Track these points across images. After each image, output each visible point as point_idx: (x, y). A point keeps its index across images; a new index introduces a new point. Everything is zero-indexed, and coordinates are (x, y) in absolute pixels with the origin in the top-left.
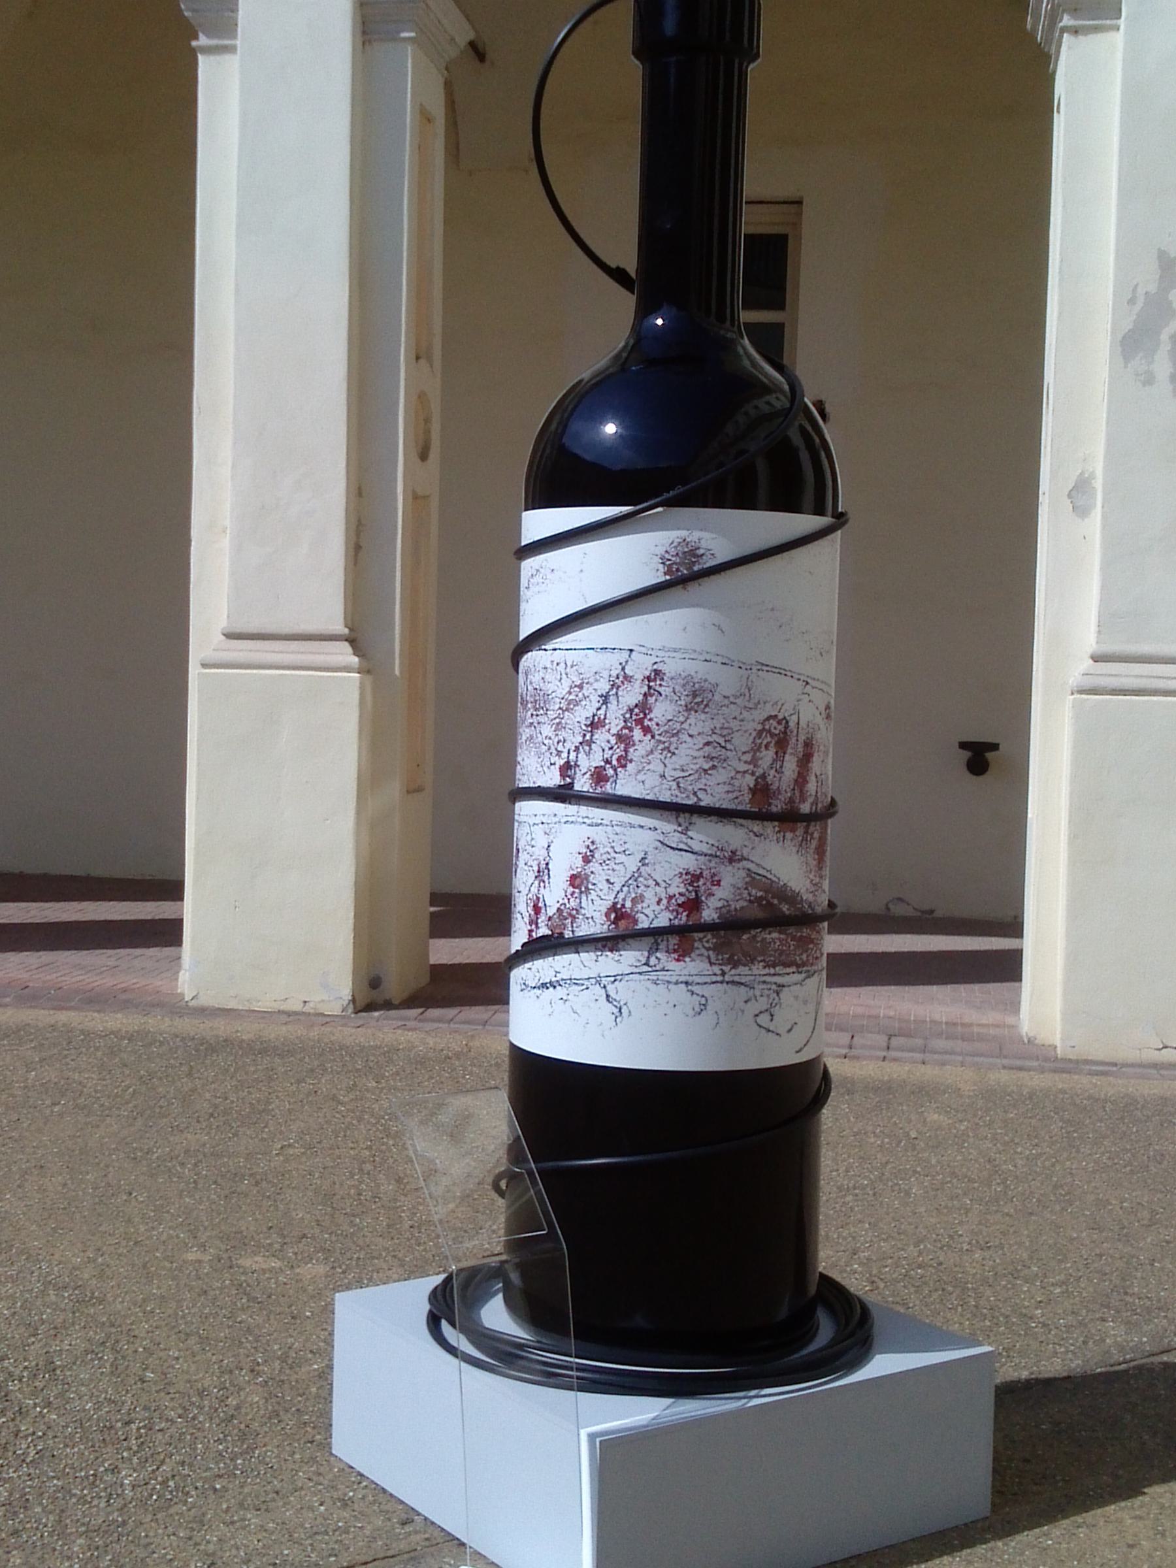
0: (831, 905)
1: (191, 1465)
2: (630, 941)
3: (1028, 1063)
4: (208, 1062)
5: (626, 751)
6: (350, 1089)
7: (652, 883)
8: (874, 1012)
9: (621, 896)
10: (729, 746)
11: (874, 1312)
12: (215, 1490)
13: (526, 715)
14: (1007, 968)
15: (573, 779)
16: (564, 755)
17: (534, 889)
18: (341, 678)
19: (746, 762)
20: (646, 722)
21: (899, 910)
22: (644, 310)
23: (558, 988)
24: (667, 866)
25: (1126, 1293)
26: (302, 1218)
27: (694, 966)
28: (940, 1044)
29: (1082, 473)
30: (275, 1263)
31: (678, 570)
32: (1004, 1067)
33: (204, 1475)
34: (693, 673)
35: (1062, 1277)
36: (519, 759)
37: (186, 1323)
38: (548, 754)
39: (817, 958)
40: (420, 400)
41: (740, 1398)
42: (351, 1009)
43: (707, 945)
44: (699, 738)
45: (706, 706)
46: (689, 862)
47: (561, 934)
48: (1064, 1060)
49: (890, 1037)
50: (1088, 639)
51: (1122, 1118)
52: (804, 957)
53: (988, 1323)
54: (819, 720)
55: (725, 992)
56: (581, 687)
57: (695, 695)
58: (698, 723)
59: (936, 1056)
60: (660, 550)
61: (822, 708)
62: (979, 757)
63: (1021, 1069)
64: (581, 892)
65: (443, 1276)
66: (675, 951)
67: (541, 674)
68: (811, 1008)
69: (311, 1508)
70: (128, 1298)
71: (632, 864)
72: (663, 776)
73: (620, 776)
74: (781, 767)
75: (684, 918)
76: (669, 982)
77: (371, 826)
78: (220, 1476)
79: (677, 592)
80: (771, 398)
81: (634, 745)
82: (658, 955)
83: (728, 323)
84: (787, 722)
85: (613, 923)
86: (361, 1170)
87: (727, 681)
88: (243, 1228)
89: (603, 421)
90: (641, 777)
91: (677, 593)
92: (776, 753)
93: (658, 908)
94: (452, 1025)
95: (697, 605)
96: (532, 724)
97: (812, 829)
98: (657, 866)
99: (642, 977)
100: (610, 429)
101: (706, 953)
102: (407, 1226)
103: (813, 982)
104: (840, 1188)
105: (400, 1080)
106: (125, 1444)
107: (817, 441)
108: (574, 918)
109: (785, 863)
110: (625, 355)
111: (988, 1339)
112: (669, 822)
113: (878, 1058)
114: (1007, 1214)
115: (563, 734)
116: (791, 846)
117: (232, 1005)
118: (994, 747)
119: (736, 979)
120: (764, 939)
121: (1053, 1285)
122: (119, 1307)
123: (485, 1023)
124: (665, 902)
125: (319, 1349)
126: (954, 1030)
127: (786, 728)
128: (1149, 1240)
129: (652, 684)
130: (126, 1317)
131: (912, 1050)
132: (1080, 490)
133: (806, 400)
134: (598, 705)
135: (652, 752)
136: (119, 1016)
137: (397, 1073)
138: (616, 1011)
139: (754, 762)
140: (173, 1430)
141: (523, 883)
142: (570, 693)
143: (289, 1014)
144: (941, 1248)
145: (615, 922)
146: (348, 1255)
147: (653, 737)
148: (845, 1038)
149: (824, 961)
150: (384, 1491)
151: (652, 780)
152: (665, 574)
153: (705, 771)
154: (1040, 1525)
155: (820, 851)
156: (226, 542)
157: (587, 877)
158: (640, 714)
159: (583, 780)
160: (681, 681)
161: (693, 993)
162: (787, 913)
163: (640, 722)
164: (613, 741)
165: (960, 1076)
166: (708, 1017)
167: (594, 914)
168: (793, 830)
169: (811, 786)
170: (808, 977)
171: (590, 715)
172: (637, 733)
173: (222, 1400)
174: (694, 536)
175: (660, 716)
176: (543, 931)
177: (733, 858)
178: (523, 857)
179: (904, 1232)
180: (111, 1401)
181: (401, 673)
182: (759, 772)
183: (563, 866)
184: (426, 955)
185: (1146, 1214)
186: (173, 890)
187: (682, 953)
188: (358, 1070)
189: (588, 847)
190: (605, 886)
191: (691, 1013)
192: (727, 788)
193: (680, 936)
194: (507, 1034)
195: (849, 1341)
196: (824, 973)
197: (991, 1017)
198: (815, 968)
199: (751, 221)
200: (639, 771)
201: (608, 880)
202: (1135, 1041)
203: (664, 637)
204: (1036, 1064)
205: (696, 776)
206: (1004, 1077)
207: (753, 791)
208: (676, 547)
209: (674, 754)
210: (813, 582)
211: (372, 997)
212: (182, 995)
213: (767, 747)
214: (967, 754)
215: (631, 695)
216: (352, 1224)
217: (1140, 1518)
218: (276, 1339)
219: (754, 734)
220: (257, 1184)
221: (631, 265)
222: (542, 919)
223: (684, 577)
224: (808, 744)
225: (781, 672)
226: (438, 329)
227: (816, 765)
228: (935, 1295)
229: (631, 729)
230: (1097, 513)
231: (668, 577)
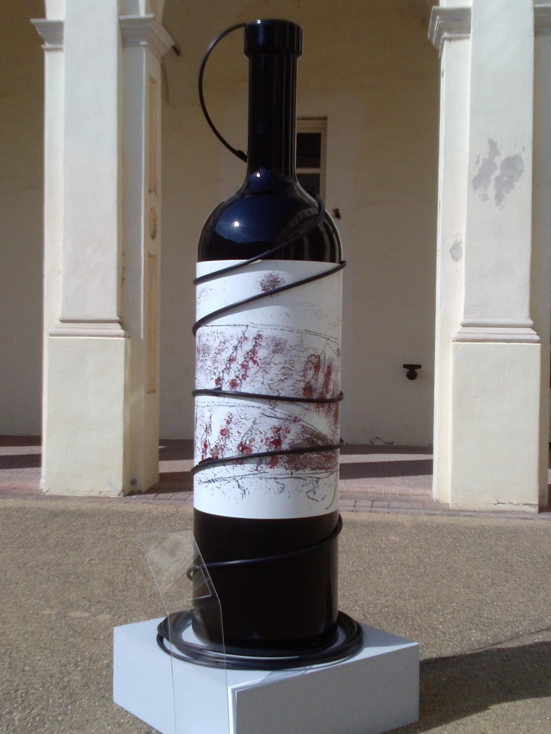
0: (341, 441)
1: (46, 710)
2: (249, 459)
3: (436, 512)
4: (54, 521)
5: (246, 372)
6: (122, 532)
7: (258, 432)
8: (365, 490)
9: (244, 439)
10: (293, 369)
11: (364, 629)
12: (58, 721)
13: (199, 356)
14: (426, 468)
15: (221, 385)
16: (217, 374)
17: (204, 437)
18: (115, 340)
19: (301, 376)
20: (255, 359)
21: (377, 443)
22: (252, 170)
23: (216, 482)
24: (265, 424)
25: (481, 617)
26: (99, 593)
27: (278, 470)
28: (395, 504)
29: (456, 241)
30: (86, 615)
31: (268, 288)
32: (425, 514)
33: (53, 714)
35: (452, 610)
36: (197, 376)
37: (44, 643)
38: (210, 374)
39: (335, 465)
40: (151, 211)
41: (302, 670)
42: (122, 494)
43: (284, 461)
45: (282, 350)
46: (275, 422)
47: (217, 457)
48: (452, 510)
49: (373, 501)
50: (460, 317)
51: (479, 536)
52: (329, 465)
53: (417, 632)
54: (334, 356)
55: (293, 482)
56: (224, 343)
58: (278, 359)
59: (394, 510)
60: (260, 280)
61: (335, 350)
62: (412, 371)
63: (432, 515)
64: (226, 438)
65: (165, 617)
66: (269, 464)
67: (206, 337)
68: (332, 488)
69: (103, 728)
70: (16, 632)
71: (249, 424)
72: (263, 383)
73: (243, 383)
75: (273, 449)
76: (267, 478)
77: (131, 409)
78: (61, 714)
79: (268, 298)
80: (310, 210)
81: (249, 369)
82: (262, 465)
83: (290, 176)
84: (319, 357)
85: (241, 451)
86: (127, 570)
87: (291, 339)
88: (71, 598)
89: (239, 219)
90: (253, 384)
91: (268, 299)
92: (315, 372)
93: (261, 444)
94: (170, 501)
96: (202, 360)
97: (332, 406)
98: (261, 425)
99: (255, 476)
101: (284, 464)
102: (148, 595)
103: (333, 477)
104: (349, 572)
105: (146, 527)
106: (15, 700)
107: (331, 229)
108: (223, 449)
109: (319, 422)
110: (243, 191)
111: (417, 640)
112: (266, 404)
113: (366, 511)
114: (426, 582)
115: (216, 365)
116: (322, 414)
117: (66, 494)
118: (419, 367)
119: (298, 476)
120: (310, 457)
121: (447, 614)
122: (12, 636)
123: (185, 500)
124: (264, 441)
125: (107, 654)
126: (402, 498)
128: (491, 592)
130: (16, 641)
131: (383, 507)
132: (455, 249)
133: (326, 210)
134: (232, 351)
135: (257, 372)
136: (12, 500)
137: (144, 524)
138: (243, 492)
139: (305, 376)
140: (38, 693)
141: (199, 434)
142: (219, 346)
143: (93, 498)
144: (396, 599)
145: (242, 451)
146: (121, 610)
147: (258, 365)
148: (352, 502)
149: (338, 467)
150: (138, 719)
151: (258, 385)
152: (263, 290)
153: (282, 380)
154: (441, 725)
155: (336, 416)
156: (60, 278)
157: (229, 430)
158: (252, 355)
160: (270, 339)
161: (278, 483)
162: (321, 445)
163: (252, 358)
164: (240, 367)
165: (404, 519)
166: (285, 494)
167: (232, 447)
168: (323, 407)
169: (331, 387)
170: (331, 474)
171: (229, 355)
172: (251, 364)
173: (61, 679)
174: (275, 273)
176: (209, 456)
177: (296, 420)
178: (199, 422)
179: (380, 592)
180: (8, 681)
181: (144, 337)
182: (307, 380)
183: (217, 426)
184: (158, 470)
185: (490, 580)
186: (37, 440)
187: (273, 464)
188: (125, 523)
189: (229, 417)
190: (237, 434)
191: (277, 492)
192: (292, 388)
193: (271, 457)
194: (192, 504)
195: (353, 642)
196: (339, 472)
197: (419, 491)
198: (334, 470)
199: (300, 128)
200: (252, 381)
201: (238, 432)
202: (484, 501)
204: (440, 512)
206: (425, 518)
207: (305, 389)
208: (267, 278)
209: (267, 373)
210: (330, 294)
211: (132, 489)
212: (42, 490)
213: (310, 369)
214: (407, 370)
215: (248, 346)
216: (123, 595)
217: (487, 720)
218: (86, 650)
219: (304, 363)
220: (78, 577)
221: (245, 149)
222: (208, 450)
223: (271, 292)
224: (329, 367)
225: (316, 334)
226: (159, 178)
227: (333, 377)
228: (394, 620)
229: (248, 362)
230: (463, 260)
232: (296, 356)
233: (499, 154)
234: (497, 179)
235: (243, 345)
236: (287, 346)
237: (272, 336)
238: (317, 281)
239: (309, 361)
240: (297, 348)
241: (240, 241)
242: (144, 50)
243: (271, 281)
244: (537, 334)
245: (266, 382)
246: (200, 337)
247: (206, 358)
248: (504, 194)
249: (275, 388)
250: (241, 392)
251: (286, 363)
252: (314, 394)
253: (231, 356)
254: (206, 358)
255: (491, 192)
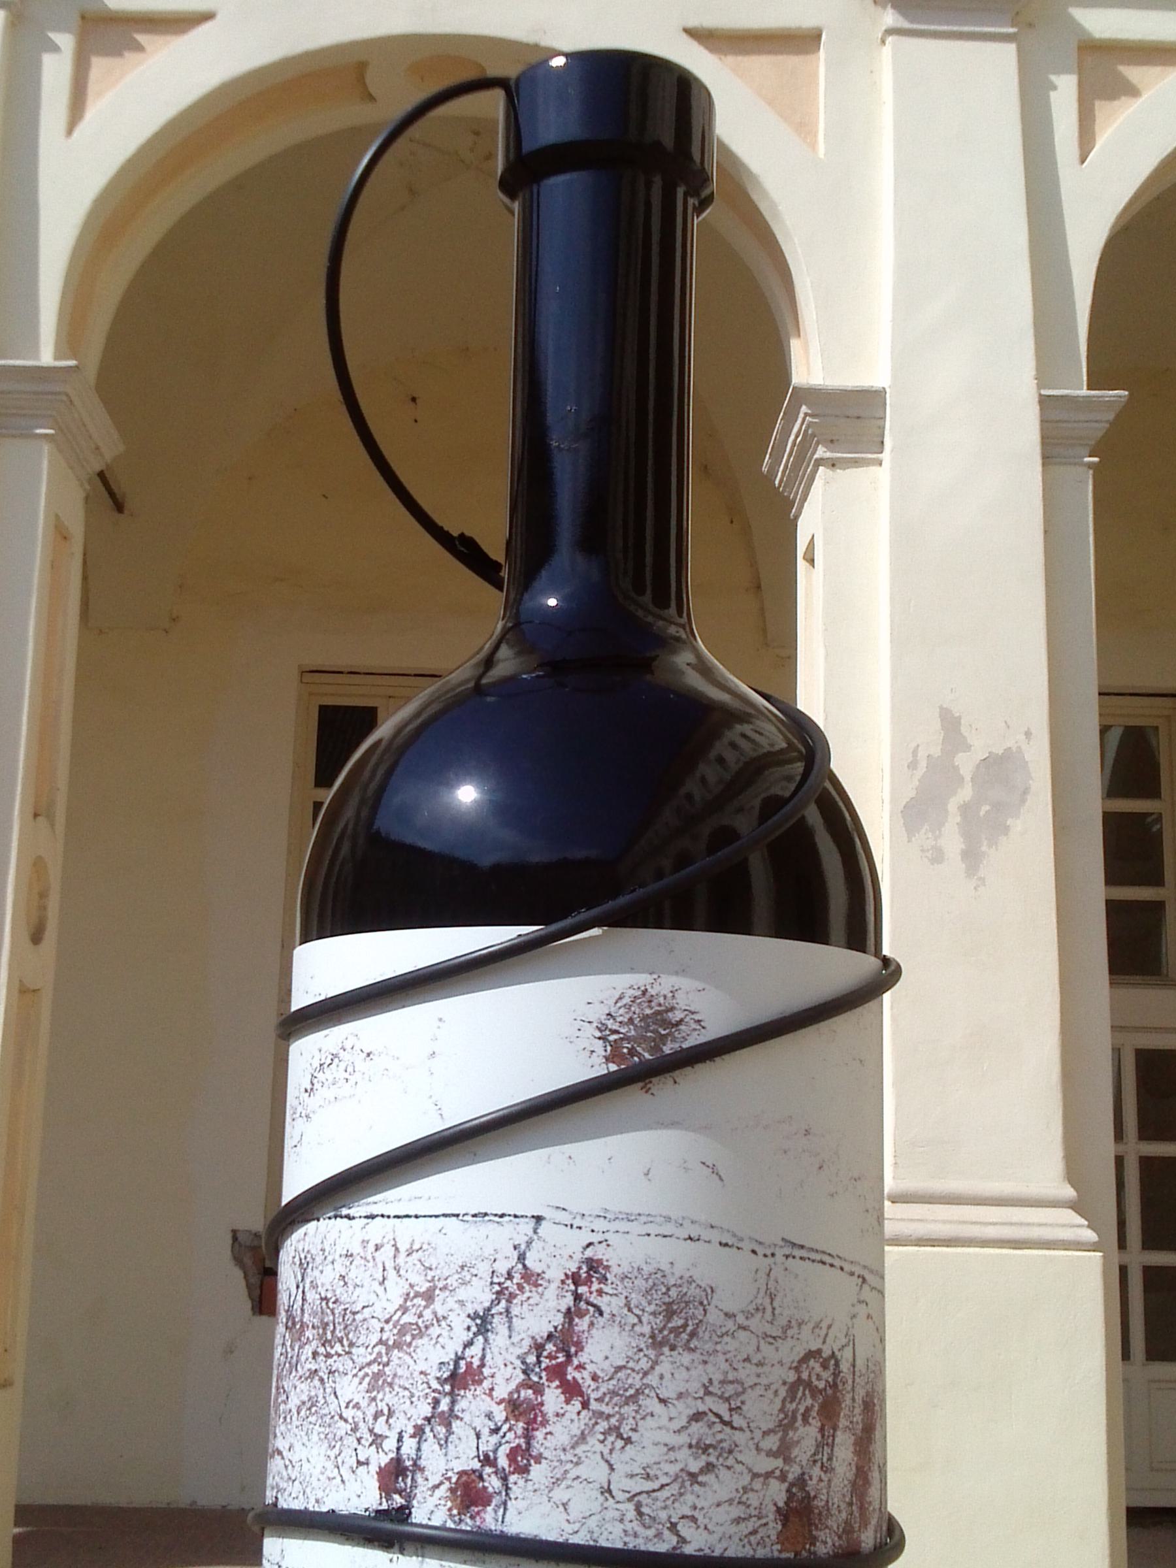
5: (528, 1436)
10: (737, 1421)
15: (409, 1498)
16: (390, 1444)
20: (571, 1373)
31: (632, 1052)
34: (665, 1267)
38: (351, 1441)
40: (36, 868)
44: (680, 1405)
45: (693, 1334)
56: (429, 1296)
57: (670, 1313)
58: (676, 1374)
60: (597, 1013)
72: (607, 1491)
73: (515, 1491)
74: (830, 1459)
79: (633, 1096)
81: (545, 1422)
84: (837, 1364)
87: (730, 1282)
90: (560, 1494)
92: (822, 1430)
95: (674, 1124)
100: (467, 794)
115: (387, 1398)
127: (836, 1375)
129: (581, 1290)
134: (467, 1336)
135: (583, 1438)
139: (784, 1452)
142: (404, 1310)
147: (585, 1405)
151: (584, 1500)
152: (608, 1059)
153: (693, 1476)
159: (433, 1501)
163: (557, 1372)
164: (500, 1413)
172: (553, 1398)
174: (664, 985)
175: (598, 1358)
182: (794, 1472)
200: (557, 1482)
203: (603, 1190)
205: (674, 1489)
207: (785, 1515)
208: (628, 1007)
209: (628, 1441)
215: (539, 1315)
219: (783, 1392)
223: (644, 1067)
229: (538, 1390)
231: (613, 1067)
232: (747, 1360)
233: (968, 748)
234: (965, 809)
235: (515, 1310)
236: (714, 1317)
237: (646, 1269)
238: (825, 1026)
239: (800, 1379)
240: (754, 1323)
241: (487, 860)
242: (46, 448)
243: (645, 1018)
244: (1089, 1226)
245: (620, 1483)
246: (303, 1266)
247: (337, 1364)
248: (984, 848)
249: (663, 1515)
250: (503, 1536)
251: (708, 1393)
252: (821, 1535)
253: (458, 1358)
254: (337, 1364)
255: (952, 842)
